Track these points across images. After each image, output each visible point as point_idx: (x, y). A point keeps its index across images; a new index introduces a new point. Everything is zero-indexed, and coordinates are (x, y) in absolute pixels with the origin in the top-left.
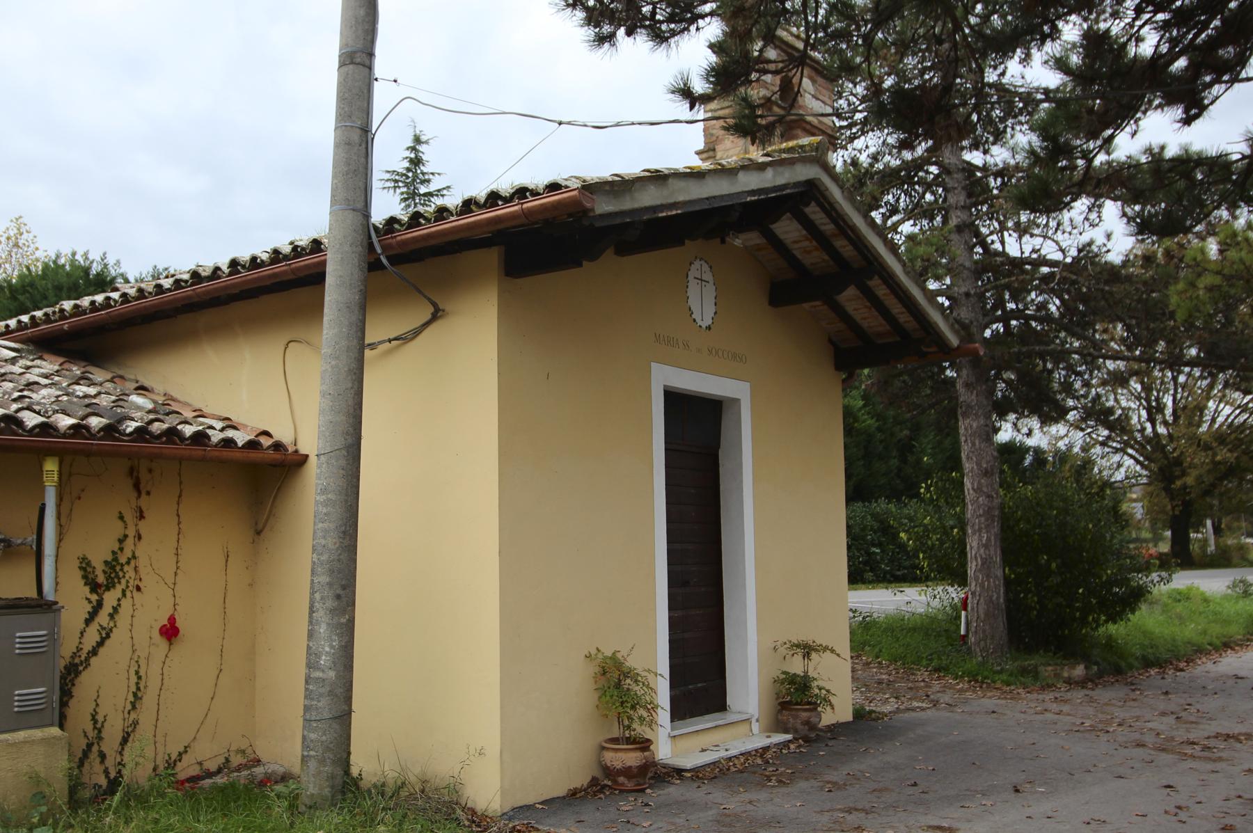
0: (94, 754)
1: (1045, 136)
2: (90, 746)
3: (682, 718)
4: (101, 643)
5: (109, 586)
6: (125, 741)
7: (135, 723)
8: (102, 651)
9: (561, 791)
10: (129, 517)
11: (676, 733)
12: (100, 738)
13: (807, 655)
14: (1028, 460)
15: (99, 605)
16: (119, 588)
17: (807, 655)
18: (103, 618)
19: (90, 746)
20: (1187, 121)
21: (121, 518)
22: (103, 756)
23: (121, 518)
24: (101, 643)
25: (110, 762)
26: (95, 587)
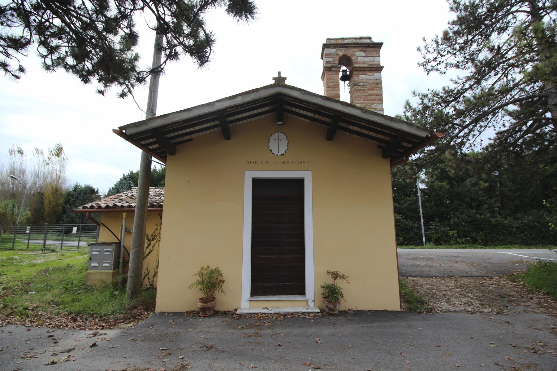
0: (146, 278)
1: (93, 66)
2: (146, 276)
3: (265, 292)
4: (150, 253)
5: (153, 240)
6: (154, 276)
7: (157, 272)
8: (150, 255)
9: (184, 310)
10: (158, 225)
11: (251, 299)
12: (148, 274)
13: (335, 278)
14: (399, 217)
15: (150, 244)
16: (155, 241)
17: (335, 278)
18: (151, 247)
19: (146, 276)
20: (122, 37)
21: (156, 225)
22: (149, 279)
23: (156, 225)
24: (150, 253)
25: (150, 280)
26: (149, 240)
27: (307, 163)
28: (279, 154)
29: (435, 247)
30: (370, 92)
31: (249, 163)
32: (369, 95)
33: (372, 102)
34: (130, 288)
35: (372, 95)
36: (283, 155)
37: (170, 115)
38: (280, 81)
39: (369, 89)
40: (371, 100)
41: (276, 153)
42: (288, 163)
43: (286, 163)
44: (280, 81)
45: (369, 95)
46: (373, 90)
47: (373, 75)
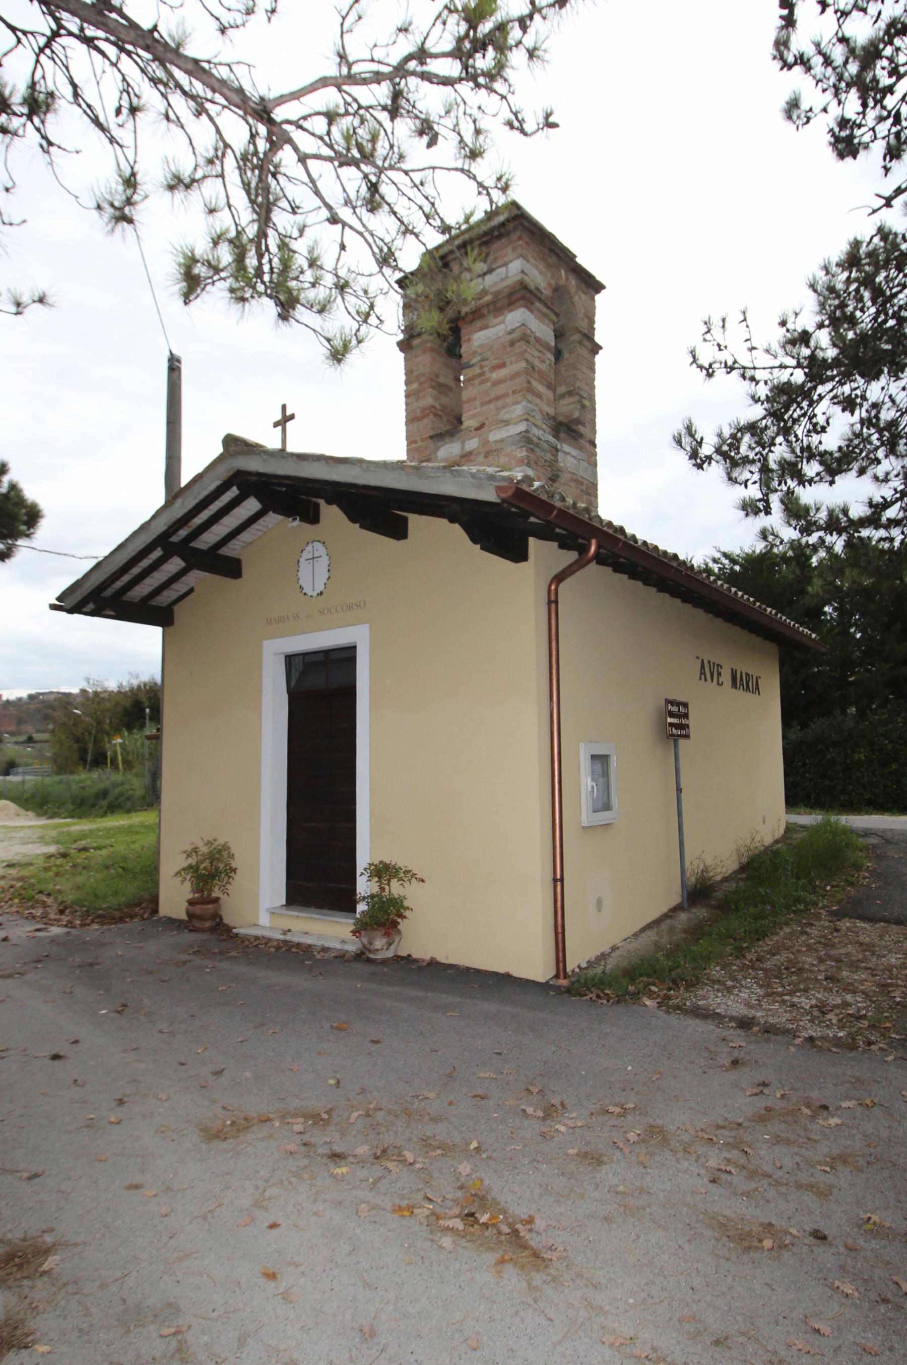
27: (362, 604)
28: (315, 594)
29: (685, 892)
30: (495, 376)
31: (269, 622)
32: (494, 384)
33: (500, 403)
34: (117, 821)
35: (500, 382)
36: (321, 593)
37: (104, 564)
38: (42, 517)
39: (494, 368)
40: (498, 398)
41: (310, 593)
42: (329, 611)
43: (326, 611)
44: (855, 239)
45: (494, 384)
46: (503, 365)
47: (503, 322)
